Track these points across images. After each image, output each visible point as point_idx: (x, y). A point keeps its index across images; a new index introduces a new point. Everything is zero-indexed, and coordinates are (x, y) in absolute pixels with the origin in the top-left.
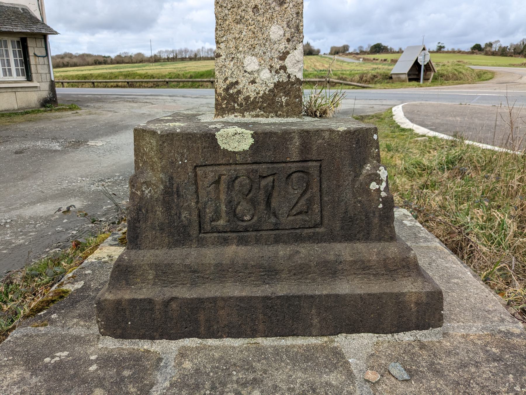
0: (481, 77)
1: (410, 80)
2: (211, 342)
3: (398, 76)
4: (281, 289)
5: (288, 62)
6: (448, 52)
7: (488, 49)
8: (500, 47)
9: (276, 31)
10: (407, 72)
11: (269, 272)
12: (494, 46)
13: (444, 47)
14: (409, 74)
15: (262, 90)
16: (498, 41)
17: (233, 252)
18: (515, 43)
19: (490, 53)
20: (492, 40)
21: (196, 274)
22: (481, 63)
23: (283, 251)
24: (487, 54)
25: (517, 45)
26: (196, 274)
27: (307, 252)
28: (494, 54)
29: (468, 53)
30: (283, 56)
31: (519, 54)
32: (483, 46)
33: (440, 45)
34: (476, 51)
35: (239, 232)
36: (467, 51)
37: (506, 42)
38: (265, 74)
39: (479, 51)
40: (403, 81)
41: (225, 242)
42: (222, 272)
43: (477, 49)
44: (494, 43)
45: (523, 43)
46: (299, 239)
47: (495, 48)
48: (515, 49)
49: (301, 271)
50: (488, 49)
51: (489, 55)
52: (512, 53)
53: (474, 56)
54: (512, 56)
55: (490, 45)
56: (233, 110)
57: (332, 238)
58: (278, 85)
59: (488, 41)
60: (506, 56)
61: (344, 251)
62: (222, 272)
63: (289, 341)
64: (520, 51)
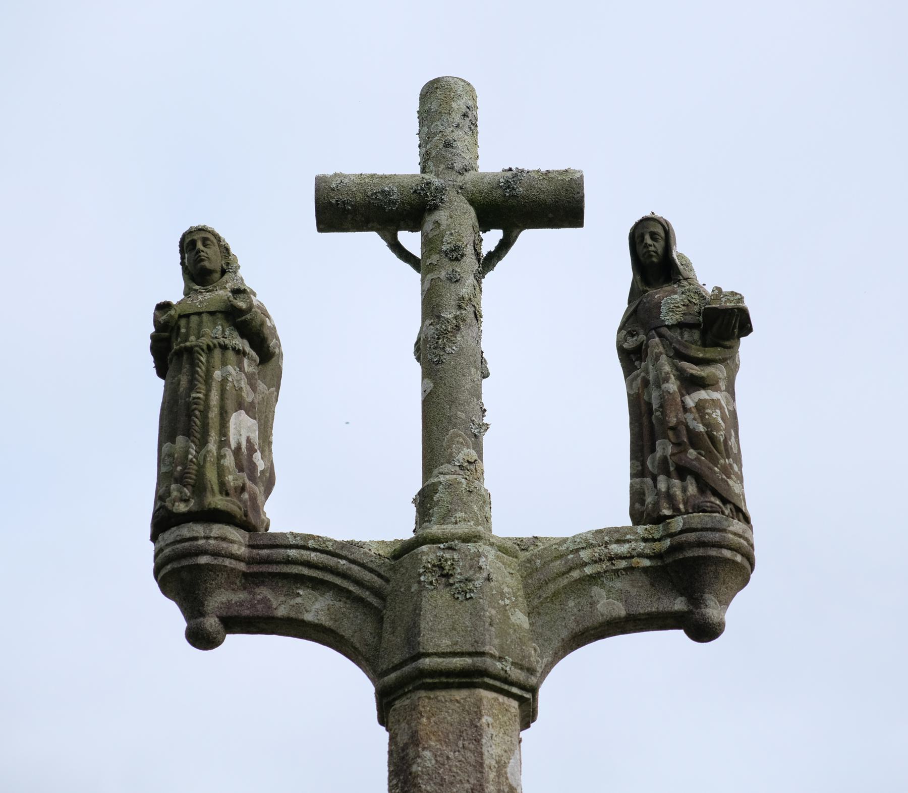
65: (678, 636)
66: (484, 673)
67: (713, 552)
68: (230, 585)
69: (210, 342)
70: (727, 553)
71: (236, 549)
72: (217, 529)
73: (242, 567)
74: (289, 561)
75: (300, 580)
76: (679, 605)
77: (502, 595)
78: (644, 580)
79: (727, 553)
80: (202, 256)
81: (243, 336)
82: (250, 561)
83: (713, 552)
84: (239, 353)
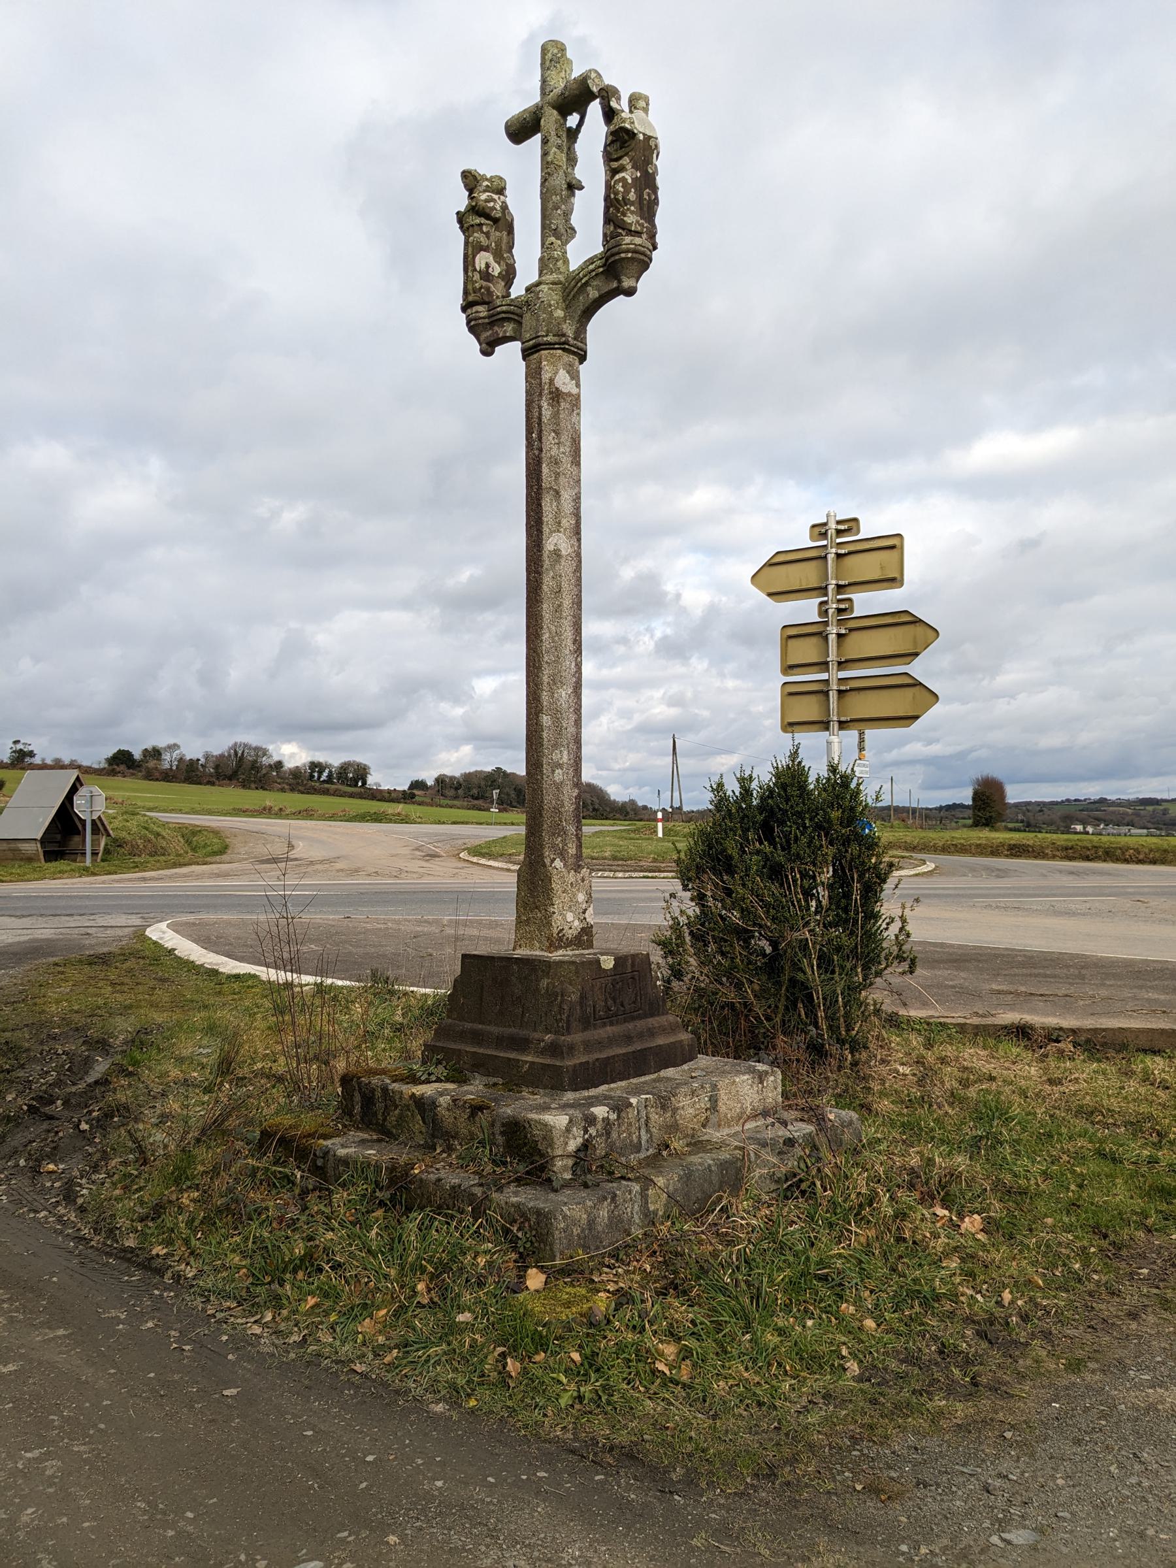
0: (203, 847)
1: (51, 856)
2: (612, 1085)
3: (12, 845)
4: (638, 1046)
5: (587, 915)
6: (44, 767)
7: (152, 764)
8: (181, 760)
9: (581, 897)
10: (39, 836)
11: (628, 1039)
12: (166, 757)
13: (31, 754)
14: (44, 841)
15: (575, 933)
16: (175, 747)
17: (610, 1030)
18: (216, 752)
19: (157, 774)
20: (161, 743)
21: (601, 1044)
22: (174, 810)
23: (630, 1026)
24: (149, 776)
25: (222, 756)
26: (601, 1044)
27: (640, 1024)
28: (168, 776)
29: (99, 772)
30: (584, 912)
31: (230, 778)
32: (137, 755)
33: (19, 746)
34: (122, 767)
35: (610, 1018)
36: (96, 766)
37: (194, 749)
38: (576, 923)
39: (129, 768)
40: (30, 859)
41: (604, 1025)
42: (612, 1041)
43: (122, 762)
44: (165, 749)
45: (236, 753)
46: (633, 1019)
47: (168, 761)
48: (217, 767)
49: (641, 1036)
50: (152, 764)
51: (157, 780)
52: (211, 775)
53: (118, 781)
54: (213, 784)
55: (156, 753)
56: (560, 947)
57: (645, 1016)
58: (582, 929)
59: (149, 745)
60: (200, 784)
61: (653, 1022)
62: (612, 1041)
63: (643, 1079)
64: (230, 772)
65: (621, 298)
66: (540, 345)
67: (617, 257)
68: (486, 330)
69: (484, 219)
70: (623, 255)
71: (482, 315)
72: (475, 309)
73: (487, 321)
74: (499, 313)
75: (503, 319)
76: (615, 285)
77: (550, 306)
78: (603, 277)
79: (623, 255)
80: (471, 180)
81: (480, 216)
82: (489, 317)
83: (617, 257)
84: (480, 225)
